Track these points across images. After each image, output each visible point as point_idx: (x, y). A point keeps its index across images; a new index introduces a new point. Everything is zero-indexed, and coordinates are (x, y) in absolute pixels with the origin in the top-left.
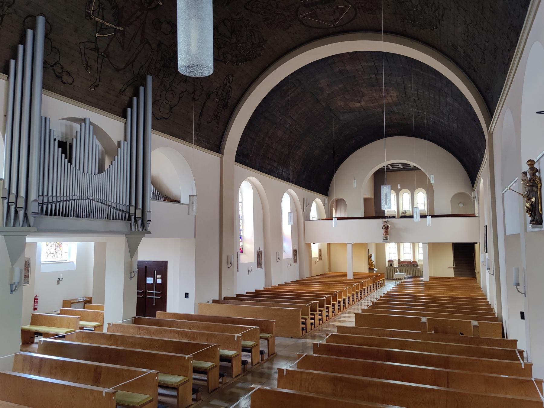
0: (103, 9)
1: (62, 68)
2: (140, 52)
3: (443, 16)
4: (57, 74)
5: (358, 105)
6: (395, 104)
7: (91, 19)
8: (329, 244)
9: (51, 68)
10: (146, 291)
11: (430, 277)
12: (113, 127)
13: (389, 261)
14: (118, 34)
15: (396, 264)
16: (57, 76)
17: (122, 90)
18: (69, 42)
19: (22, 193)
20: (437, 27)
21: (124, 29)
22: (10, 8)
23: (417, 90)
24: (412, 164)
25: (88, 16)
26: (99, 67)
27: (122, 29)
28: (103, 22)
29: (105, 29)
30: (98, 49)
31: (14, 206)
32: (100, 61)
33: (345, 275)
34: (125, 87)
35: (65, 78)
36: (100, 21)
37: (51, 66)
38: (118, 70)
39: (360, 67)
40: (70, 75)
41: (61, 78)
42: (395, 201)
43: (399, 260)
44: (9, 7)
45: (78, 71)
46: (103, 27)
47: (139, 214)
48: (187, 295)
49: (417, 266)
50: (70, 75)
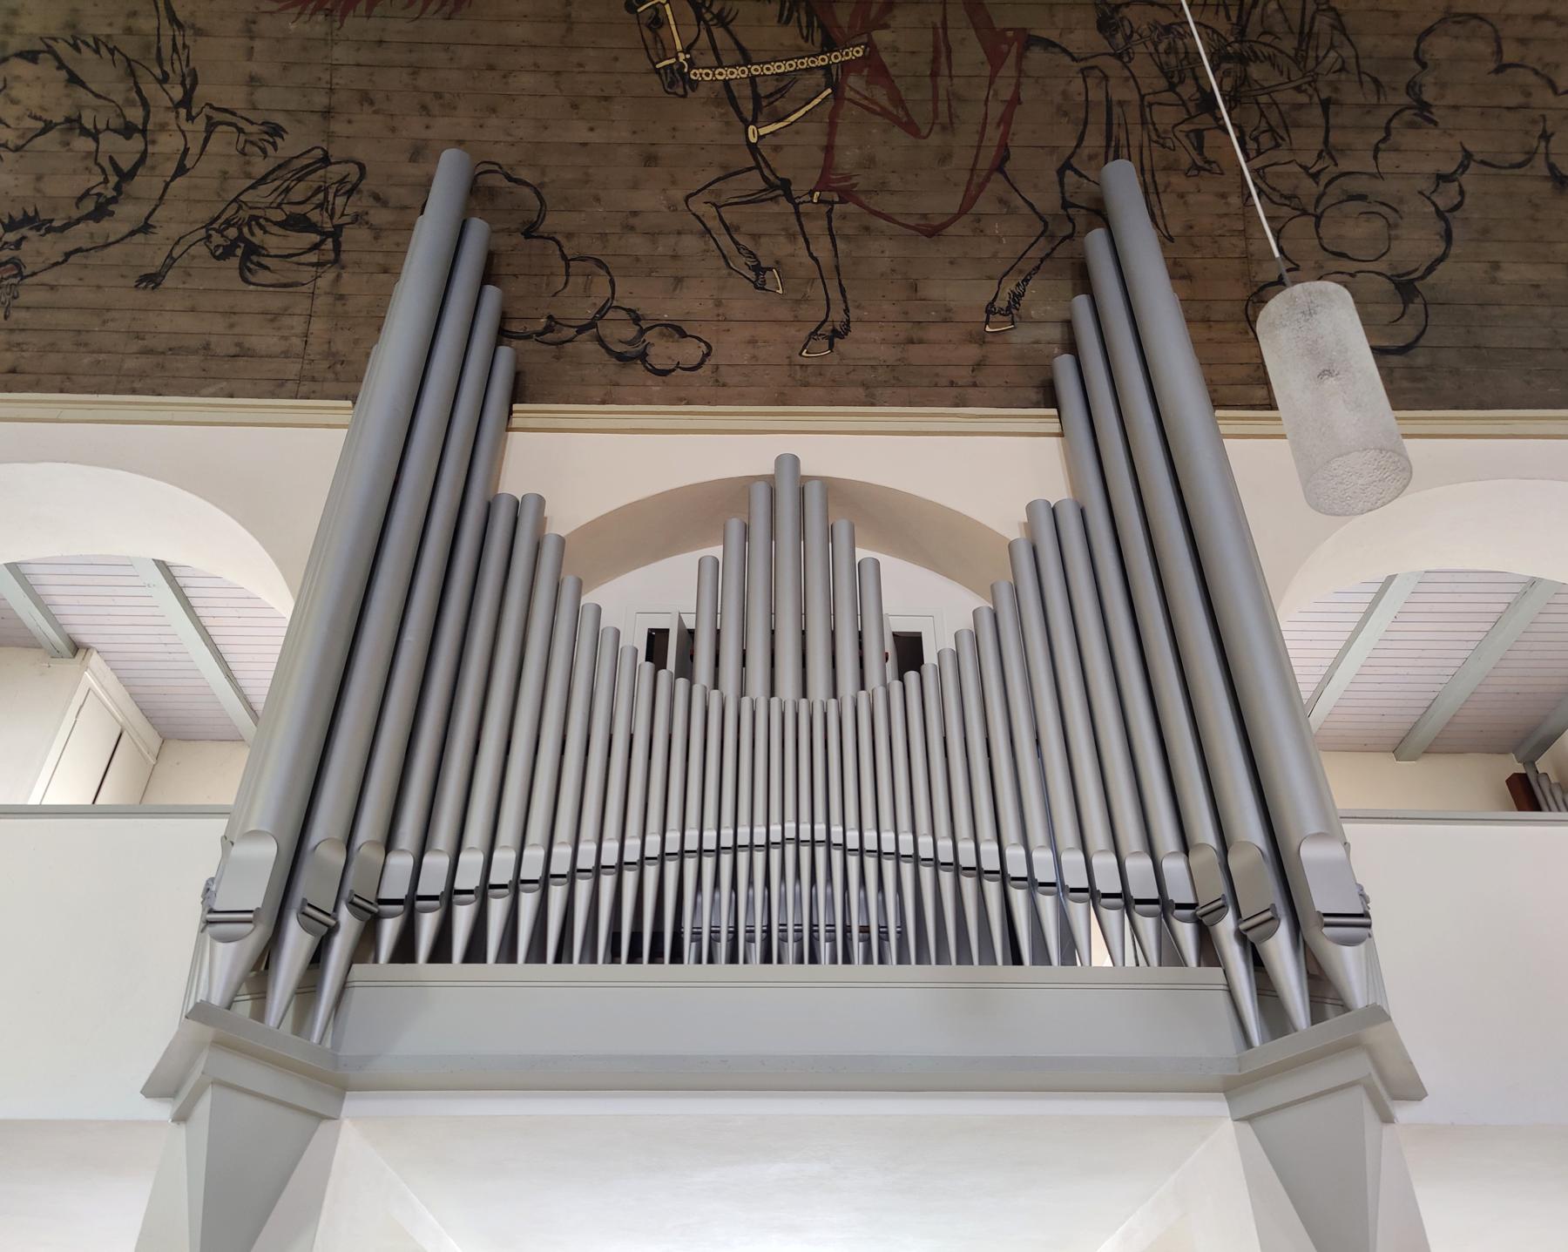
0: (723, 21)
1: (636, 319)
2: (1016, 101)
4: (619, 348)
7: (694, 85)
9: (584, 336)
12: (995, 471)
14: (853, 80)
16: (622, 358)
17: (1002, 303)
18: (635, 213)
21: (870, 45)
22: (355, 197)
25: (678, 81)
26: (822, 248)
27: (857, 52)
28: (755, 70)
29: (781, 92)
30: (786, 185)
31: (1283, 933)
32: (816, 227)
34: (1009, 286)
35: (663, 351)
36: (738, 73)
37: (581, 330)
38: (932, 231)
40: (683, 335)
41: (643, 356)
44: (349, 193)
45: (718, 304)
46: (763, 91)
50: (683, 335)
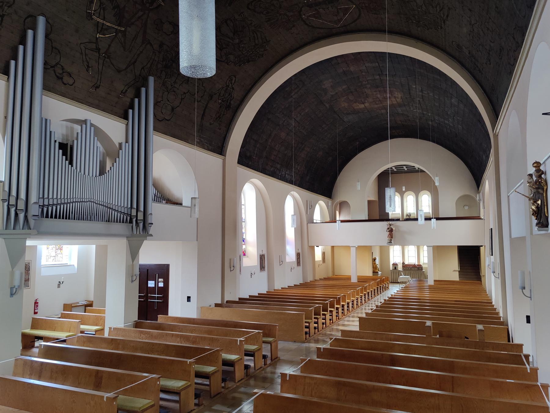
0: (104, 9)
1: (63, 69)
2: (141, 52)
3: (447, 16)
4: (58, 75)
5: (362, 106)
6: (400, 105)
7: (92, 19)
8: (333, 247)
9: (52, 69)
10: (147, 294)
11: (435, 281)
12: (114, 128)
13: (393, 264)
14: (120, 34)
15: (400, 268)
16: (57, 77)
17: (124, 91)
18: (69, 42)
19: (23, 195)
20: (441, 28)
21: (126, 29)
22: (10, 8)
23: (422, 91)
24: (417, 166)
25: (89, 16)
26: (100, 68)
27: (123, 29)
28: (105, 22)
29: (106, 29)
30: (99, 49)
32: (101, 61)
33: (349, 278)
34: (126, 88)
35: (66, 79)
36: (101, 21)
37: (52, 67)
38: (119, 71)
39: (364, 68)
40: (71, 76)
41: (62, 79)
42: (400, 203)
43: (403, 263)
44: (9, 7)
45: (79, 72)
46: (104, 27)
47: (141, 216)
48: (189, 299)
49: (422, 269)
50: (71, 76)
